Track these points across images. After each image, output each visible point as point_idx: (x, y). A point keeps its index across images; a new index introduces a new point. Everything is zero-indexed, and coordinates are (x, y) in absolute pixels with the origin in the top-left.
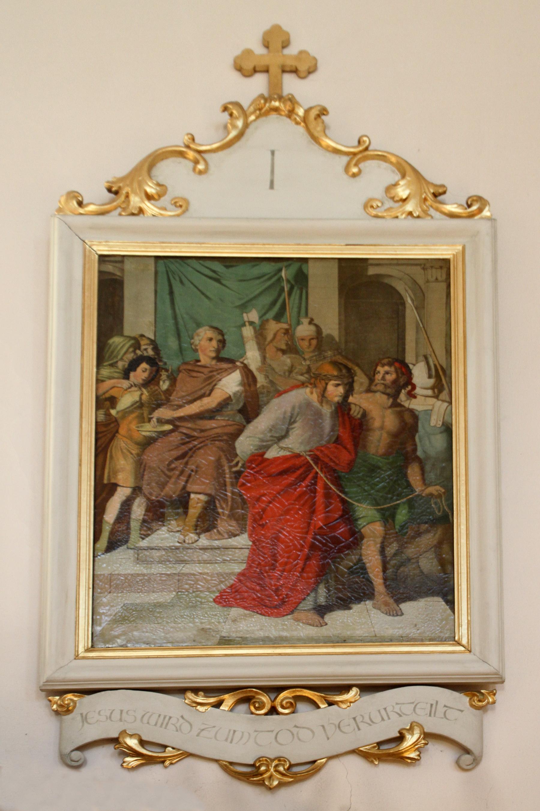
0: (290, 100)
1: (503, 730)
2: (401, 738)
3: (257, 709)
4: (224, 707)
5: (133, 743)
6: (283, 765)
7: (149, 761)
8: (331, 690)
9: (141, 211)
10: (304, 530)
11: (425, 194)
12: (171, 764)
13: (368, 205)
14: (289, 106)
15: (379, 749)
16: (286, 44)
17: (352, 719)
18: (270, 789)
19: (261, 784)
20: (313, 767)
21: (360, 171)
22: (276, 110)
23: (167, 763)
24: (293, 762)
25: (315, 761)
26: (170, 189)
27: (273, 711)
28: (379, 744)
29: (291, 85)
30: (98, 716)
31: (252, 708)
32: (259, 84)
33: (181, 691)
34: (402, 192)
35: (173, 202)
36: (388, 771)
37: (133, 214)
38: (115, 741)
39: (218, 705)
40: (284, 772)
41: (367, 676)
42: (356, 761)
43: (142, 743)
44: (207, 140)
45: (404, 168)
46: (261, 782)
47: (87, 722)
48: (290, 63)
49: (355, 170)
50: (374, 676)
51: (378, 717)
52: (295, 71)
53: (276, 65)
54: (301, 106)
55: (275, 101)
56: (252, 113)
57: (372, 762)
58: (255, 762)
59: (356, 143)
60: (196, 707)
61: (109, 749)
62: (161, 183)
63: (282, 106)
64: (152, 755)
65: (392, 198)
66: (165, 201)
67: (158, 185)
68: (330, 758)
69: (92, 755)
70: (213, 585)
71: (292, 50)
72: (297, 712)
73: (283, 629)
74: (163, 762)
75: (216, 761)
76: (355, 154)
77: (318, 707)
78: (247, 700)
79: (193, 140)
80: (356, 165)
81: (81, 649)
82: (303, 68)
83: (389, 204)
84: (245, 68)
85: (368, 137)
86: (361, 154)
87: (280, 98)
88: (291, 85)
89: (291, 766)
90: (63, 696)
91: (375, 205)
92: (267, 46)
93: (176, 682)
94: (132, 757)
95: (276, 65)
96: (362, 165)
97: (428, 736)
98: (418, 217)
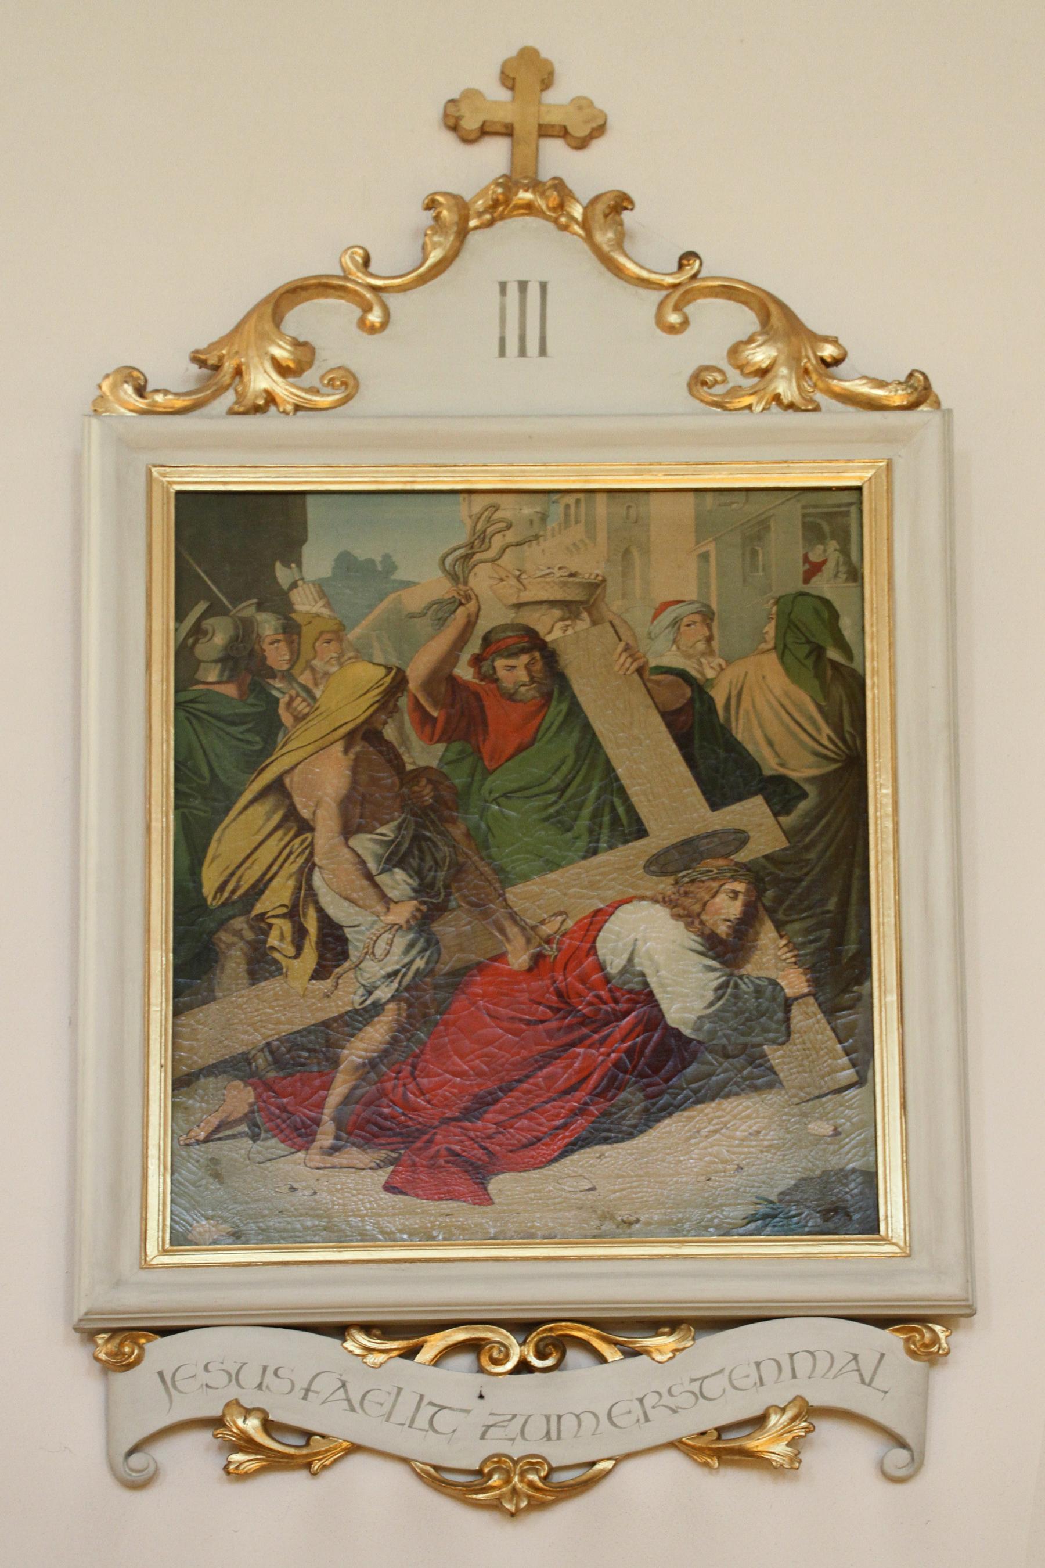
0: (555, 187)
1: (970, 1394)
2: (759, 1421)
3: (496, 1362)
4: (426, 1355)
5: (252, 1426)
6: (537, 1471)
7: (277, 1462)
8: (627, 1328)
9: (271, 399)
10: (421, 944)
11: (805, 361)
12: (324, 1467)
13: (698, 381)
14: (554, 197)
15: (719, 1438)
16: (547, 81)
17: (788, 1356)
18: (513, 1515)
19: (495, 1506)
20: (586, 1480)
21: (686, 322)
22: (529, 208)
23: (316, 1466)
24: (554, 1465)
25: (593, 1464)
26: (320, 354)
27: (523, 1367)
28: (720, 1430)
29: (556, 159)
30: (191, 1370)
31: (485, 1361)
32: (493, 158)
33: (339, 1331)
34: (761, 355)
35: (326, 382)
36: (733, 1484)
37: (257, 409)
38: (217, 1423)
39: (410, 1354)
40: (540, 1484)
41: (446, 1305)
42: (673, 1459)
43: (269, 1426)
44: (393, 258)
45: (773, 315)
46: (495, 1503)
47: (237, 1380)
48: (553, 118)
49: (674, 318)
50: (485, 1304)
51: (724, 1376)
52: (564, 133)
53: (525, 152)
54: (578, 201)
55: (526, 191)
56: (480, 214)
57: (706, 1464)
58: (484, 1462)
59: (675, 267)
60: (364, 1356)
61: (205, 1437)
62: (301, 339)
63: (541, 203)
64: (289, 1450)
65: (741, 368)
66: (311, 377)
67: (297, 344)
68: (618, 1460)
69: (163, 1453)
70: (510, 1148)
71: (558, 96)
72: (564, 1369)
73: (555, 1209)
74: (309, 1466)
75: (405, 1461)
76: (675, 286)
77: (602, 1360)
78: (474, 1346)
79: (367, 261)
80: (677, 308)
81: (152, 1249)
82: (586, 132)
83: (735, 378)
84: (461, 125)
85: (701, 264)
86: (686, 286)
87: (535, 185)
88: (556, 159)
89: (552, 1470)
90: (120, 1340)
91: (709, 379)
92: (508, 80)
93: (378, 1312)
94: (247, 1453)
95: (525, 152)
96: (689, 309)
97: (809, 1413)
98: (791, 406)
